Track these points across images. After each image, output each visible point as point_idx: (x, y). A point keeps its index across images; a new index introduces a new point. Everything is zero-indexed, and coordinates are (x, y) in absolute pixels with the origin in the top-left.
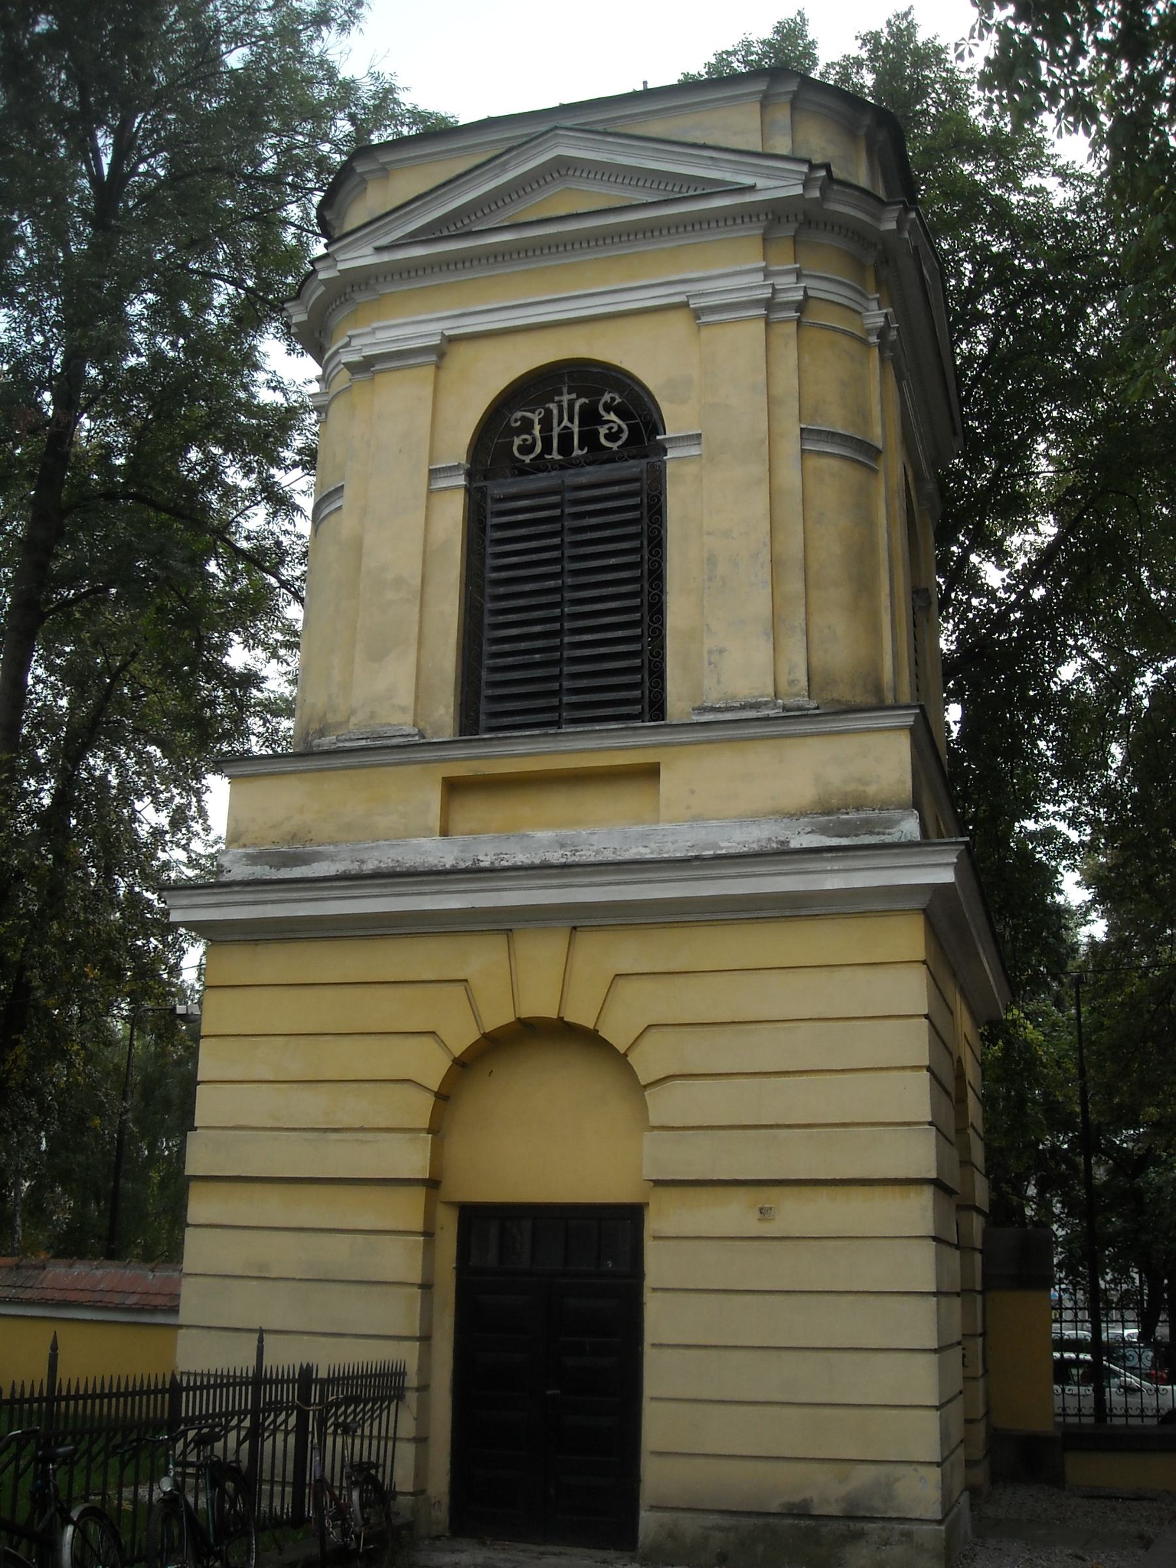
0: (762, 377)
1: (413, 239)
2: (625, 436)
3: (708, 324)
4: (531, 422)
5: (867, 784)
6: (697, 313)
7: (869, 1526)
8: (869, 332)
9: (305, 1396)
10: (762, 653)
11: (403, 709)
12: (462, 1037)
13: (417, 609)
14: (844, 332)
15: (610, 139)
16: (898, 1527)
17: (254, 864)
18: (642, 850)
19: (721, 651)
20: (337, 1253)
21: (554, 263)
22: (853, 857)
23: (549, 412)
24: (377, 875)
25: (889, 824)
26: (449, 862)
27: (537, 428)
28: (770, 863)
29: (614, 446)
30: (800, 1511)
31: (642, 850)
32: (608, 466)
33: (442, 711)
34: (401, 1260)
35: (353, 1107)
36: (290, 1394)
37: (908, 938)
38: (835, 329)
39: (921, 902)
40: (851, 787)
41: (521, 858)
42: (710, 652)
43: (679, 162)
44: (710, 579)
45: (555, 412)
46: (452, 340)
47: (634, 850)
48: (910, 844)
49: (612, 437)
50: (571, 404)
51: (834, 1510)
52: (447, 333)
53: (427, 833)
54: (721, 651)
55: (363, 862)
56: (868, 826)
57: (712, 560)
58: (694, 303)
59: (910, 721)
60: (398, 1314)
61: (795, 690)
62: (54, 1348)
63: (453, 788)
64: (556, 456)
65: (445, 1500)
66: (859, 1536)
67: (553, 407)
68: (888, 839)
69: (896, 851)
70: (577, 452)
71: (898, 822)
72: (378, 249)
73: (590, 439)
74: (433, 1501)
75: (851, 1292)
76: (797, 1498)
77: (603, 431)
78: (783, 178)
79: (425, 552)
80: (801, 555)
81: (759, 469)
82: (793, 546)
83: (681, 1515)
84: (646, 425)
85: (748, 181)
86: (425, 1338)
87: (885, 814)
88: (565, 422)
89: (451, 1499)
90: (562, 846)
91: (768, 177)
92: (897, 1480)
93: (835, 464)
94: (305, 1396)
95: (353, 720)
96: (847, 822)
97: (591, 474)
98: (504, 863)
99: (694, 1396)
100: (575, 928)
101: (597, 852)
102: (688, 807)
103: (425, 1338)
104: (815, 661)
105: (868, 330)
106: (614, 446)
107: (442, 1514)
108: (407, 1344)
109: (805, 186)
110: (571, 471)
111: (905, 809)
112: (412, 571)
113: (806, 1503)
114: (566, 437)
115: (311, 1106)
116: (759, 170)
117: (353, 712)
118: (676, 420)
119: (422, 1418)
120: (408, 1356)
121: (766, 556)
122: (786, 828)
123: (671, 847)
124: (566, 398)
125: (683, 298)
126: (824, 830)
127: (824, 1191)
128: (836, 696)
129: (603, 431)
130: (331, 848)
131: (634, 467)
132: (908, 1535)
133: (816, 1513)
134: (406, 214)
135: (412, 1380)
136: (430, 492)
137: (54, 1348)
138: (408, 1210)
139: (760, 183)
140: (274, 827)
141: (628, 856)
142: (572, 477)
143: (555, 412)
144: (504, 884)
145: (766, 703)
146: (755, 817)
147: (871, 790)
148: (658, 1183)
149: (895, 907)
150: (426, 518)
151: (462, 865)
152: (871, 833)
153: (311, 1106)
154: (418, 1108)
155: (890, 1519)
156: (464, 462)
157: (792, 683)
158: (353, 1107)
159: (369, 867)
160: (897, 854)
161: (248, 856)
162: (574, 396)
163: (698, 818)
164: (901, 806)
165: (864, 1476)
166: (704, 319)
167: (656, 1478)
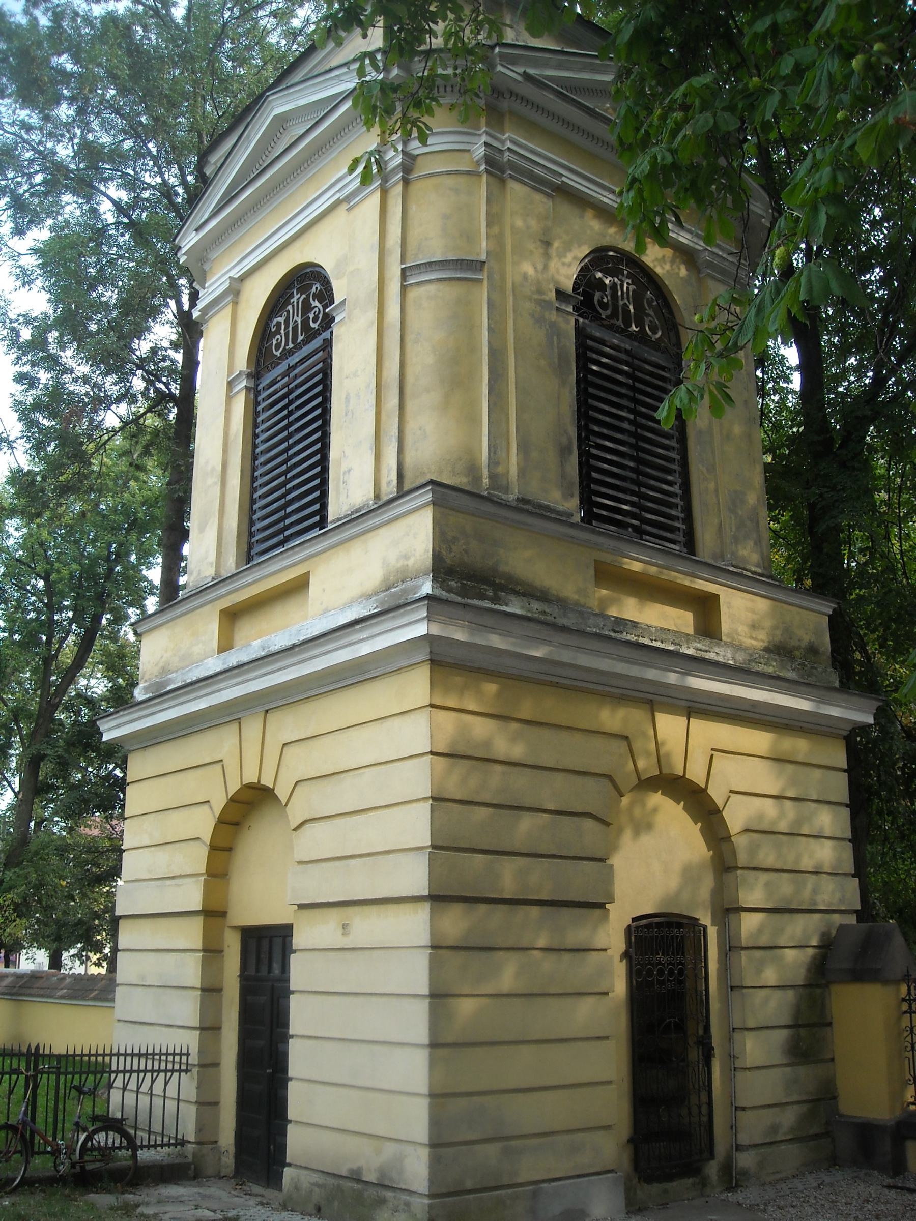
7: (389, 1194)
8: (478, 164)
14: (449, 173)
15: (291, 90)
21: (286, 195)
25: (419, 587)
28: (332, 641)
30: (355, 1177)
34: (190, 971)
37: (416, 686)
38: (439, 174)
39: (424, 655)
43: (326, 88)
59: (429, 497)
60: (187, 1009)
62: (607, 1038)
65: (232, 1150)
66: (382, 1201)
69: (392, 614)
72: (197, 230)
74: (223, 1150)
75: (376, 994)
76: (354, 1166)
77: (311, 316)
83: (304, 1172)
89: (236, 1147)
96: (395, 593)
99: (307, 1077)
100: (267, 711)
102: (322, 604)
105: (477, 161)
107: (229, 1161)
114: (295, 328)
127: (374, 909)
132: (407, 1204)
133: (364, 1179)
134: (208, 198)
137: (607, 1038)
138: (191, 934)
144: (221, 685)
146: (349, 605)
147: (411, 562)
148: (301, 906)
149: (413, 661)
154: (196, 859)
160: (394, 617)
165: (390, 1149)
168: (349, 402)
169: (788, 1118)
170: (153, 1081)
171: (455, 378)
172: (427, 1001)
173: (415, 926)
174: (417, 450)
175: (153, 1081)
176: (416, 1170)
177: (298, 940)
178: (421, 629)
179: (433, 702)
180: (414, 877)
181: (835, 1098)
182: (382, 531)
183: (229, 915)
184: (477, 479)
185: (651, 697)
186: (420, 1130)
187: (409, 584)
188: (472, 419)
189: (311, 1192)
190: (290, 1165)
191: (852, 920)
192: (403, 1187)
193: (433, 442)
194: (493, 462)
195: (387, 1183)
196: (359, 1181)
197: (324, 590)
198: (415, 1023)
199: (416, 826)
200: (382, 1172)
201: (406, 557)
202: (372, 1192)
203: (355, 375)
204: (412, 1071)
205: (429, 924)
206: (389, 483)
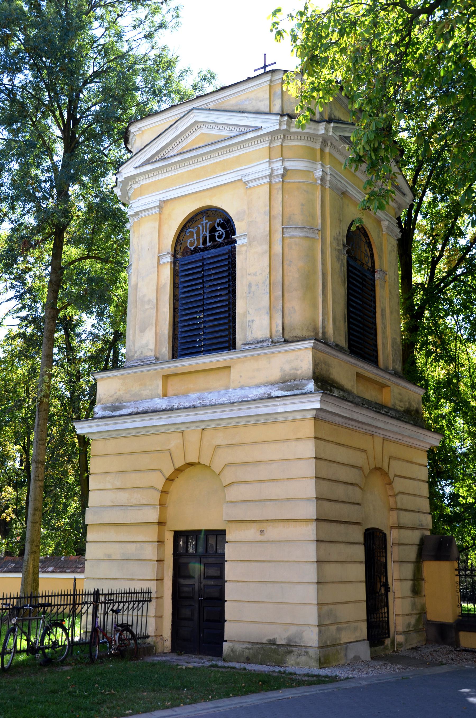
0: (268, 208)
1: (148, 162)
2: (224, 236)
3: (250, 188)
4: (193, 232)
5: (298, 370)
6: (246, 183)
7: (294, 649)
9: (96, 601)
10: (266, 320)
11: (151, 350)
12: (169, 471)
13: (155, 312)
16: (304, 649)
17: (105, 411)
18: (224, 399)
19: (253, 321)
20: (131, 549)
22: (286, 400)
23: (199, 228)
24: (143, 413)
25: (304, 385)
26: (164, 407)
27: (195, 235)
29: (220, 240)
30: (272, 642)
31: (224, 399)
32: (219, 249)
33: (164, 349)
34: (150, 552)
35: (137, 497)
36: (91, 599)
40: (292, 372)
41: (187, 404)
42: (249, 322)
44: (249, 293)
45: (201, 228)
46: (165, 201)
47: (221, 400)
48: (310, 393)
49: (220, 237)
50: (206, 224)
51: (283, 642)
52: (162, 200)
53: (158, 396)
54: (253, 321)
55: (138, 408)
56: (297, 387)
57: (250, 285)
58: (245, 179)
59: (312, 345)
60: (150, 571)
61: (278, 334)
63: (166, 377)
64: (202, 246)
65: (170, 639)
66: (290, 652)
67: (200, 226)
68: (303, 391)
70: (208, 244)
71: (307, 385)
73: (212, 238)
76: (271, 638)
77: (217, 234)
78: (271, 123)
79: (157, 289)
80: (281, 280)
81: (266, 247)
82: (278, 276)
84: (231, 231)
85: (259, 125)
86: (160, 580)
87: (303, 382)
88: (204, 232)
90: (199, 399)
91: (267, 122)
92: (304, 631)
93: (297, 240)
94: (96, 601)
95: (136, 355)
96: (290, 385)
97: (213, 252)
98: (181, 406)
101: (210, 401)
102: (240, 382)
103: (160, 580)
104: (286, 322)
106: (220, 240)
107: (168, 644)
108: (153, 582)
109: (280, 124)
110: (206, 252)
111: (310, 379)
112: (153, 296)
113: (274, 640)
115: (123, 497)
116: (263, 120)
117: (135, 352)
118: (239, 226)
119: (159, 607)
120: (152, 586)
121: (268, 282)
122: (270, 389)
123: (233, 398)
124: (204, 222)
125: (240, 178)
126: (282, 389)
128: (294, 335)
129: (217, 234)
130: (128, 404)
131: (227, 248)
133: (278, 643)
135: (154, 595)
136: (159, 265)
139: (264, 125)
140: (111, 396)
141: (220, 402)
142: (207, 254)
143: (201, 228)
145: (266, 340)
147: (299, 372)
150: (158, 275)
151: (168, 408)
152: (298, 389)
153: (123, 497)
155: (302, 646)
156: (170, 252)
157: (277, 331)
158: (137, 497)
159: (140, 410)
161: (103, 408)
162: (207, 221)
163: (242, 387)
164: (309, 379)
165: (292, 630)
166: (250, 185)
167: (229, 630)
168: (251, 287)
169: (413, 620)
170: (88, 608)
171: (308, 287)
172: (315, 565)
173: (310, 531)
174: (291, 317)
175: (88, 608)
176: (311, 638)
177: (229, 537)
178: (318, 406)
179: (317, 436)
180: (310, 511)
181: (425, 613)
182: (280, 355)
183: (168, 523)
184: (317, 334)
185: (373, 433)
186: (314, 620)
187: (298, 382)
188: (315, 306)
189: (243, 652)
190: (226, 641)
191: (428, 533)
192: (303, 645)
193: (297, 313)
194: (324, 327)
195: (292, 644)
196: (275, 644)
197: (241, 376)
198: (311, 573)
199: (309, 489)
200: (289, 639)
201: (296, 369)
202: (284, 649)
203: (255, 274)
204: (310, 594)
205: (315, 532)
206: (277, 331)
